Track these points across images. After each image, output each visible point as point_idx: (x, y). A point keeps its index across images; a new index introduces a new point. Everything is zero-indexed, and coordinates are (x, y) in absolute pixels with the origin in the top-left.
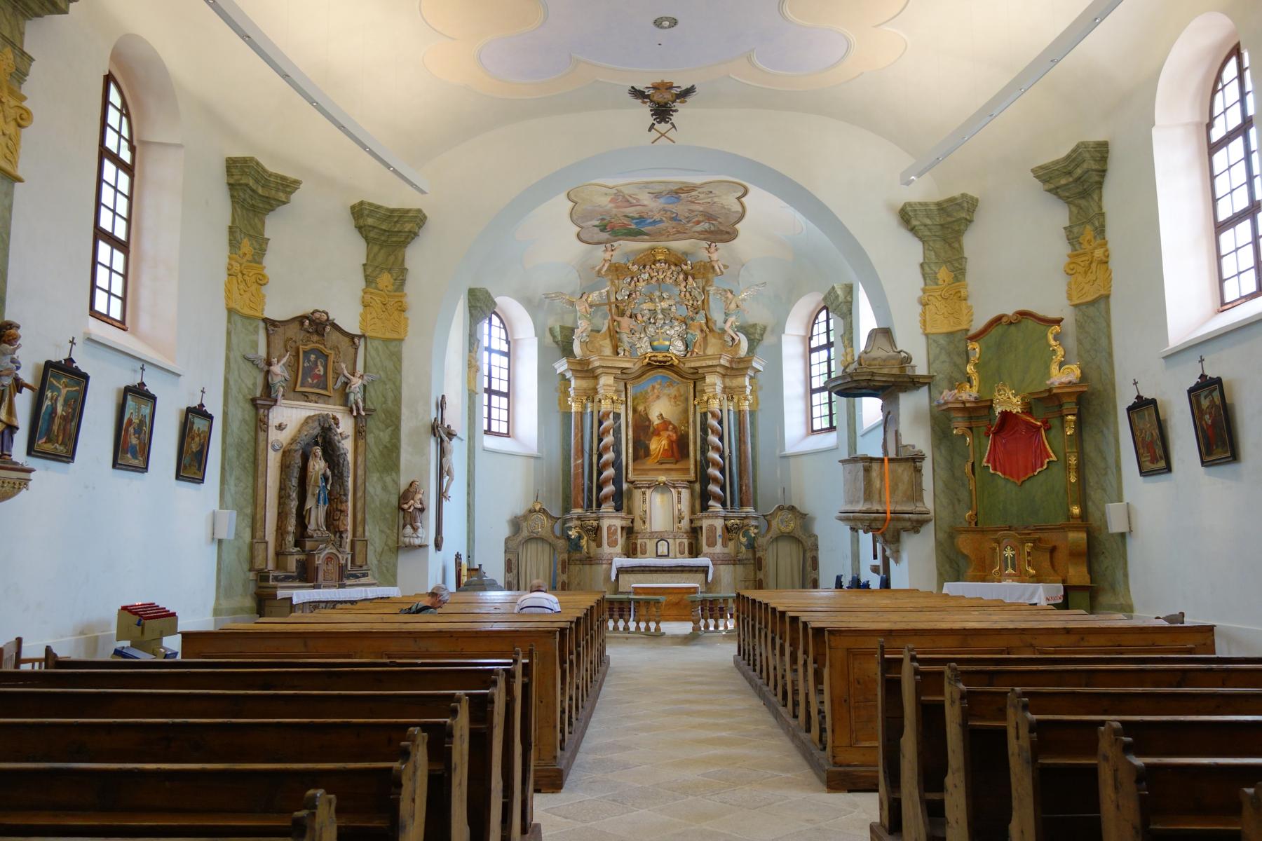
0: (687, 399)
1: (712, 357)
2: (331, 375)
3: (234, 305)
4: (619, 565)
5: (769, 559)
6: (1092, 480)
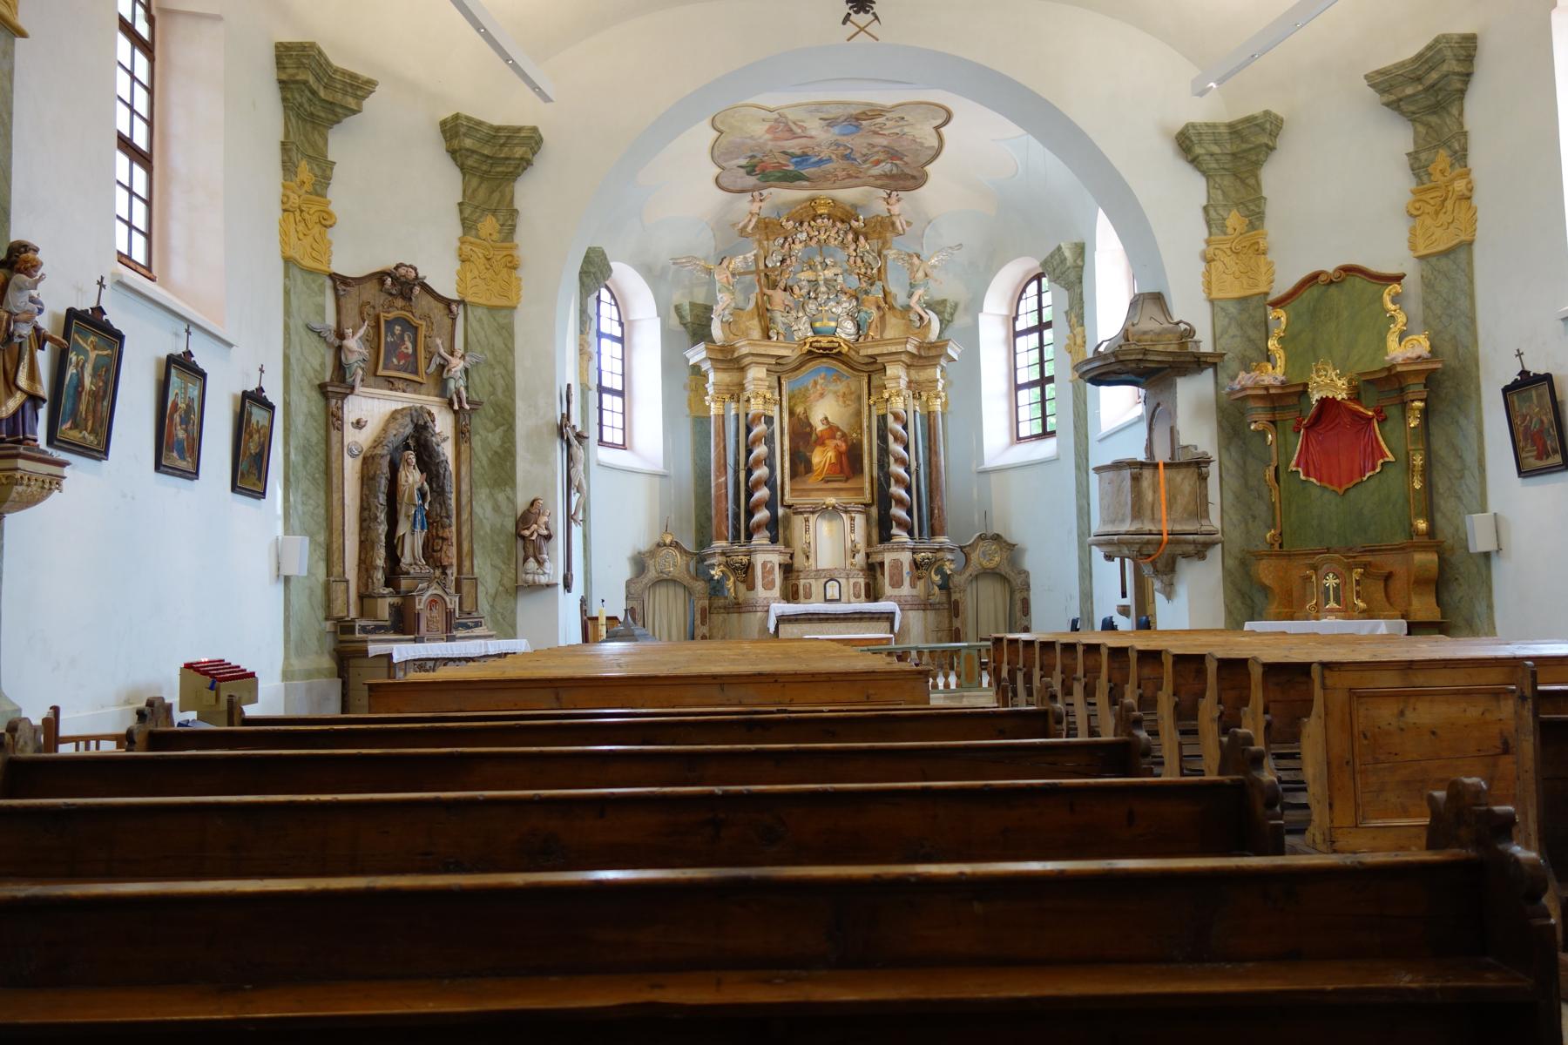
0: (859, 398)
1: (893, 341)
2: (422, 354)
3: (291, 253)
4: (779, 612)
5: (968, 601)
6: (1441, 484)
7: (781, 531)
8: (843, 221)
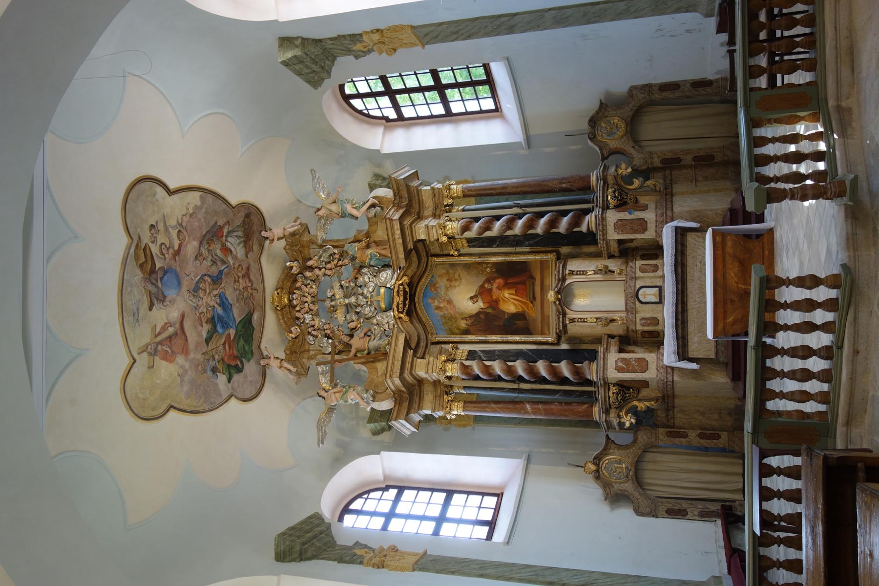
0: (453, 265)
1: (390, 231)
7: (585, 346)
8: (296, 281)
